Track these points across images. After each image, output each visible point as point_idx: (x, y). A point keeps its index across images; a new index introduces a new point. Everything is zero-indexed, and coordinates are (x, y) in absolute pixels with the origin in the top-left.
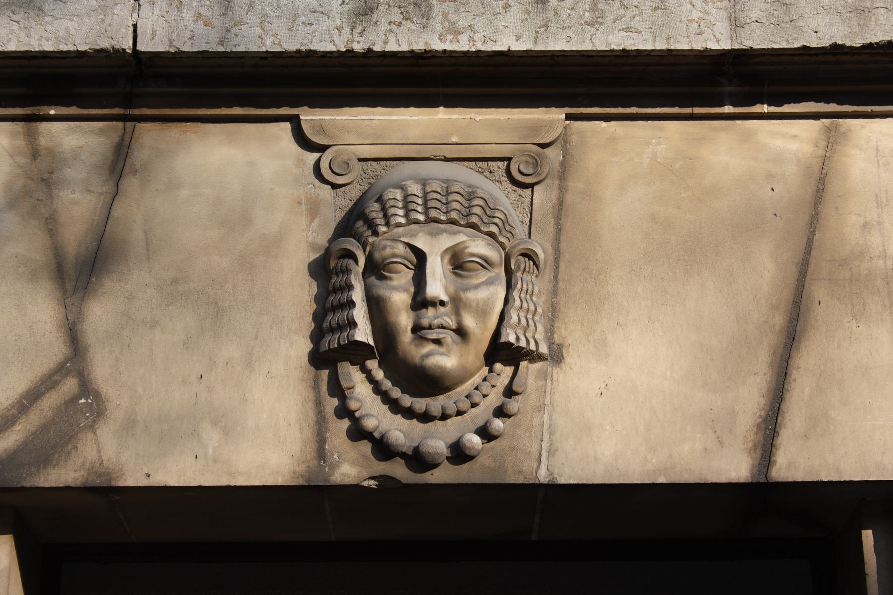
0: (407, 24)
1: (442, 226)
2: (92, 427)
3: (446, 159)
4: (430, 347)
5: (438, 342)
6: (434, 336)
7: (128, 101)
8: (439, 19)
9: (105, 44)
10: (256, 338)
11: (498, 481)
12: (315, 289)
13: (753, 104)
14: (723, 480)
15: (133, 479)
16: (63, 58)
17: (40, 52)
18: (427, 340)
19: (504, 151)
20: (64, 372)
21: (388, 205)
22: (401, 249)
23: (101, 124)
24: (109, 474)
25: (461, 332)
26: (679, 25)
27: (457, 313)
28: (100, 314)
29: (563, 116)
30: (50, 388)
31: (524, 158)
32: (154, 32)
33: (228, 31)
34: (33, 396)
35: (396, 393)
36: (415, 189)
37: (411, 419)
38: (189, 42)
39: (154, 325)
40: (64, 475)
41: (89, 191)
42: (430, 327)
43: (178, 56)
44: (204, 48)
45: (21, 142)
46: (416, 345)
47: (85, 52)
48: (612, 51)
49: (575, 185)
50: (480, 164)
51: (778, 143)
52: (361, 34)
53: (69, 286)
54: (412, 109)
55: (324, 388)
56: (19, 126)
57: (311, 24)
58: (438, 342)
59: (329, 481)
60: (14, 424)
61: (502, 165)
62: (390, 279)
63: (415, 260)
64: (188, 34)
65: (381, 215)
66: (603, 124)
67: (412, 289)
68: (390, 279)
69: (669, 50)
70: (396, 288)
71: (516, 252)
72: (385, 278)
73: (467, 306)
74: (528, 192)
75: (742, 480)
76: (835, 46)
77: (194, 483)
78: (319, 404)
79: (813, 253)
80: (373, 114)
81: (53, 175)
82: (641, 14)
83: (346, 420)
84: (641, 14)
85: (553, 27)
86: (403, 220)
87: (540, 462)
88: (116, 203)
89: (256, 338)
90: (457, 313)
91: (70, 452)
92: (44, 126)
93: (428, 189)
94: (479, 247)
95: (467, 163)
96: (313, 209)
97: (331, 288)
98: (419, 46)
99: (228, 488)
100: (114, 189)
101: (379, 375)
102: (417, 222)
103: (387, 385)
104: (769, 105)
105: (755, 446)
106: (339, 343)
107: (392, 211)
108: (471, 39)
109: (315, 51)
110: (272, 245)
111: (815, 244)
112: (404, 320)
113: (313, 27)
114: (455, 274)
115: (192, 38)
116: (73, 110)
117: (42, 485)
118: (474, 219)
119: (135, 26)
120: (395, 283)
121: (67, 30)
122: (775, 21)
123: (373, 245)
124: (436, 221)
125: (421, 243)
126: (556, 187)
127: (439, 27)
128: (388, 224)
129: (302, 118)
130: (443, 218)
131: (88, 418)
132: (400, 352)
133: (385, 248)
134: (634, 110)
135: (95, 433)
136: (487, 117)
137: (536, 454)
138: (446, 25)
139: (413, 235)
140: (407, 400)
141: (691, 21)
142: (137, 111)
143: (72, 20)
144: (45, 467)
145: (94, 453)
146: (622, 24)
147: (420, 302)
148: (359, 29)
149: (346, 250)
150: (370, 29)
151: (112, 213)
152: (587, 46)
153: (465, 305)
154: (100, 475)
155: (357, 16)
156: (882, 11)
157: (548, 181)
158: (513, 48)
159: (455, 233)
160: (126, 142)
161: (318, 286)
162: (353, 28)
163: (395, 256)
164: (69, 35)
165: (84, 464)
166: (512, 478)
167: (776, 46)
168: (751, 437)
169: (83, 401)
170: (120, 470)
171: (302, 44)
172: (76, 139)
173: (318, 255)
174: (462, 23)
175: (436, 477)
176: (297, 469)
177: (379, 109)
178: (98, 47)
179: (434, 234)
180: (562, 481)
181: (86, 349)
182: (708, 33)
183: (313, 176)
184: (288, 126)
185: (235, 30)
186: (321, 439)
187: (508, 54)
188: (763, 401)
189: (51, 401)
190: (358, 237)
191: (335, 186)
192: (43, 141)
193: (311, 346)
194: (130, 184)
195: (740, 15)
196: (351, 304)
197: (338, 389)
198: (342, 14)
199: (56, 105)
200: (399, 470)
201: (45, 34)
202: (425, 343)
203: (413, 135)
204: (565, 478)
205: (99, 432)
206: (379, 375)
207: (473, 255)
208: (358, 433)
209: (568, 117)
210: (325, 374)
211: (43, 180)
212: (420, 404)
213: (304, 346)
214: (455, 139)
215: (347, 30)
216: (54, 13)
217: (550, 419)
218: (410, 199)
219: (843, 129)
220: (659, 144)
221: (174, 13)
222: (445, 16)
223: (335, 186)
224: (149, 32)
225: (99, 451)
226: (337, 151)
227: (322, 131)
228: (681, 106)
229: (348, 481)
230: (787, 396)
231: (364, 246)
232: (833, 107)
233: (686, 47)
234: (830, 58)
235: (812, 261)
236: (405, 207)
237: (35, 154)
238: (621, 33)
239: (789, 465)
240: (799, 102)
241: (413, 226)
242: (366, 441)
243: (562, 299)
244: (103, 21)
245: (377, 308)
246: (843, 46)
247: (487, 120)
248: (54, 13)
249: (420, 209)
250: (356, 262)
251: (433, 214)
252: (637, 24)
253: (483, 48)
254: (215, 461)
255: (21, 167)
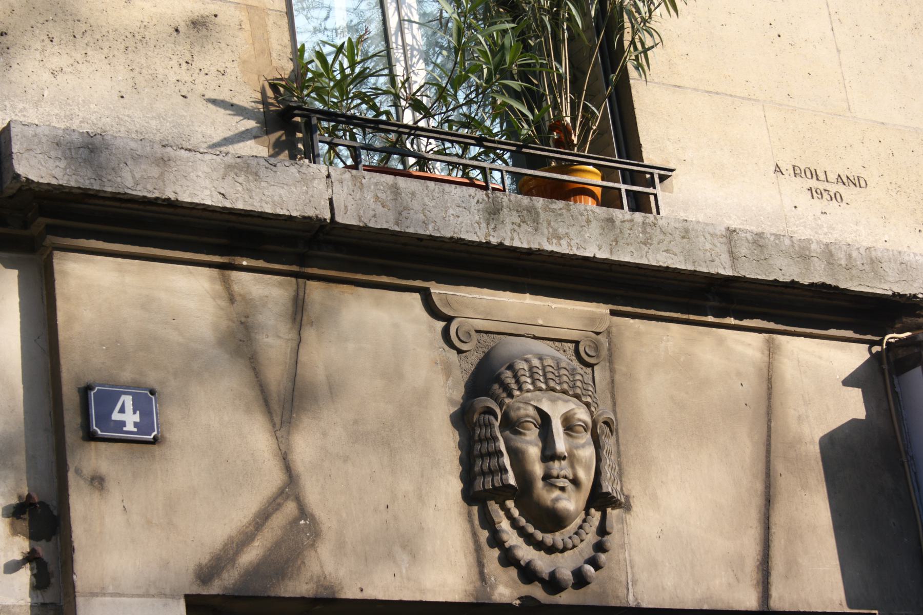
0: (524, 225)
1: (557, 394)
2: (313, 546)
3: (535, 338)
4: (556, 493)
5: (563, 489)
6: (561, 485)
7: (302, 260)
8: (545, 224)
9: (311, 213)
10: (422, 476)
11: (604, 604)
12: (458, 438)
13: (725, 317)
14: (743, 608)
15: (350, 593)
16: (193, 208)
17: (261, 212)
18: (556, 486)
19: (574, 335)
20: (284, 495)
21: (519, 374)
22: (531, 411)
23: (279, 278)
24: (332, 587)
25: (576, 482)
26: (699, 252)
27: (572, 466)
28: (305, 447)
29: (608, 311)
30: (277, 509)
31: (588, 343)
32: (346, 207)
33: (400, 214)
34: (263, 517)
35: (531, 529)
36: (536, 362)
37: (540, 550)
38: (373, 220)
39: (346, 459)
40: (299, 587)
41: (279, 337)
42: (558, 477)
43: (365, 230)
44: (385, 226)
45: (218, 287)
46: (547, 491)
47: (296, 217)
48: (660, 266)
49: (620, 367)
50: (557, 343)
51: (740, 348)
52: (494, 229)
53: (277, 420)
54: (508, 293)
55: (477, 522)
56: (215, 272)
57: (458, 217)
58: (563, 489)
59: (490, 599)
60: (253, 540)
61: (572, 346)
62: (524, 434)
63: (540, 421)
64: (372, 213)
65: (513, 381)
66: (631, 321)
67: (540, 444)
68: (524, 434)
69: (695, 271)
70: (529, 443)
71: (601, 419)
72: (520, 433)
73: (579, 461)
74: (589, 370)
75: (754, 609)
76: (793, 282)
77: (396, 598)
78: (475, 535)
79: (772, 436)
80: (482, 294)
81: (249, 320)
82: (675, 240)
83: (496, 549)
84: (675, 240)
85: (621, 242)
86: (531, 387)
87: (628, 589)
88: (301, 350)
89: (422, 476)
90: (572, 466)
91: (300, 567)
92: (235, 274)
93: (546, 364)
94: (582, 415)
95: (548, 342)
96: (447, 370)
97: (476, 437)
98: (535, 246)
99: (421, 602)
100: (298, 337)
101: (516, 513)
102: (540, 389)
103: (523, 521)
104: (735, 319)
105: (758, 583)
106: (493, 485)
107: (523, 379)
108: (569, 245)
109: (463, 240)
110: (423, 397)
111: (773, 429)
112: (538, 469)
113: (460, 219)
114: (568, 434)
115: (375, 216)
116: (261, 264)
117: (283, 595)
118: (578, 391)
119: (331, 201)
120: (528, 438)
121: (281, 197)
122: (755, 257)
123: (508, 406)
124: (553, 390)
125: (546, 407)
126: (607, 368)
127: (546, 232)
128: (520, 389)
129: (432, 291)
130: (558, 388)
131: (308, 538)
132: (535, 496)
133: (519, 409)
134: (652, 312)
135: (316, 551)
136: (559, 306)
137: (625, 583)
138: (551, 230)
139: (539, 400)
140: (539, 535)
141: (706, 250)
142: (310, 270)
143: (283, 188)
144: (283, 579)
145: (318, 568)
146: (663, 246)
147: (549, 455)
148: (492, 226)
149: (488, 407)
150: (499, 227)
151: (300, 358)
152: (644, 261)
153: (578, 460)
154: (326, 588)
155: (489, 214)
156: (816, 259)
157: (602, 363)
158: (598, 256)
159: (567, 401)
160: (301, 297)
161: (460, 435)
162: (488, 224)
163: (527, 416)
164: (283, 201)
165: (312, 577)
166: (613, 603)
167: (760, 277)
168: (755, 575)
169: (302, 522)
170: (340, 584)
171: (454, 233)
172: (264, 289)
173: (456, 409)
174: (561, 231)
175: (566, 598)
176: (467, 588)
177: (485, 290)
178: (306, 215)
179: (553, 401)
180: (644, 605)
181: (298, 476)
182: (717, 262)
183: (442, 341)
184: (417, 296)
185: (405, 214)
186: (480, 564)
187: (592, 260)
188: (306, 501)
189: (278, 521)
190: (496, 398)
191: (460, 352)
192: (236, 288)
193: (462, 485)
194: (309, 334)
195: (734, 249)
196: (499, 453)
197: (488, 522)
198: (478, 211)
199: (247, 257)
200: (537, 591)
201: (264, 198)
202: (554, 489)
203: (513, 315)
204: (647, 603)
205: (319, 550)
206: (516, 513)
207: (580, 420)
208: (508, 558)
209: (613, 313)
210: (475, 509)
211: (242, 323)
212: (549, 538)
213: (455, 486)
214: (540, 322)
215: (484, 225)
216: (268, 179)
217: (630, 556)
218: (535, 370)
219: (777, 342)
220: (668, 341)
221: (358, 194)
222: (549, 224)
223: (460, 352)
224: (343, 207)
225: (322, 567)
226: (460, 322)
227: (448, 304)
228: (682, 313)
229: (505, 600)
230: (772, 545)
231: (501, 405)
232: (772, 325)
233: (705, 270)
234: (233, 218)
235: (773, 442)
236: (531, 376)
237: (232, 299)
238: (664, 254)
239: (780, 598)
240: (752, 318)
241: (538, 393)
242: (512, 567)
243: (624, 460)
244: (307, 193)
245: (517, 456)
246: (797, 283)
247: (560, 308)
248: (268, 179)
249: (541, 378)
250: (497, 419)
251: (552, 384)
252: (672, 246)
253: (578, 253)
254: (409, 579)
255: (222, 309)
